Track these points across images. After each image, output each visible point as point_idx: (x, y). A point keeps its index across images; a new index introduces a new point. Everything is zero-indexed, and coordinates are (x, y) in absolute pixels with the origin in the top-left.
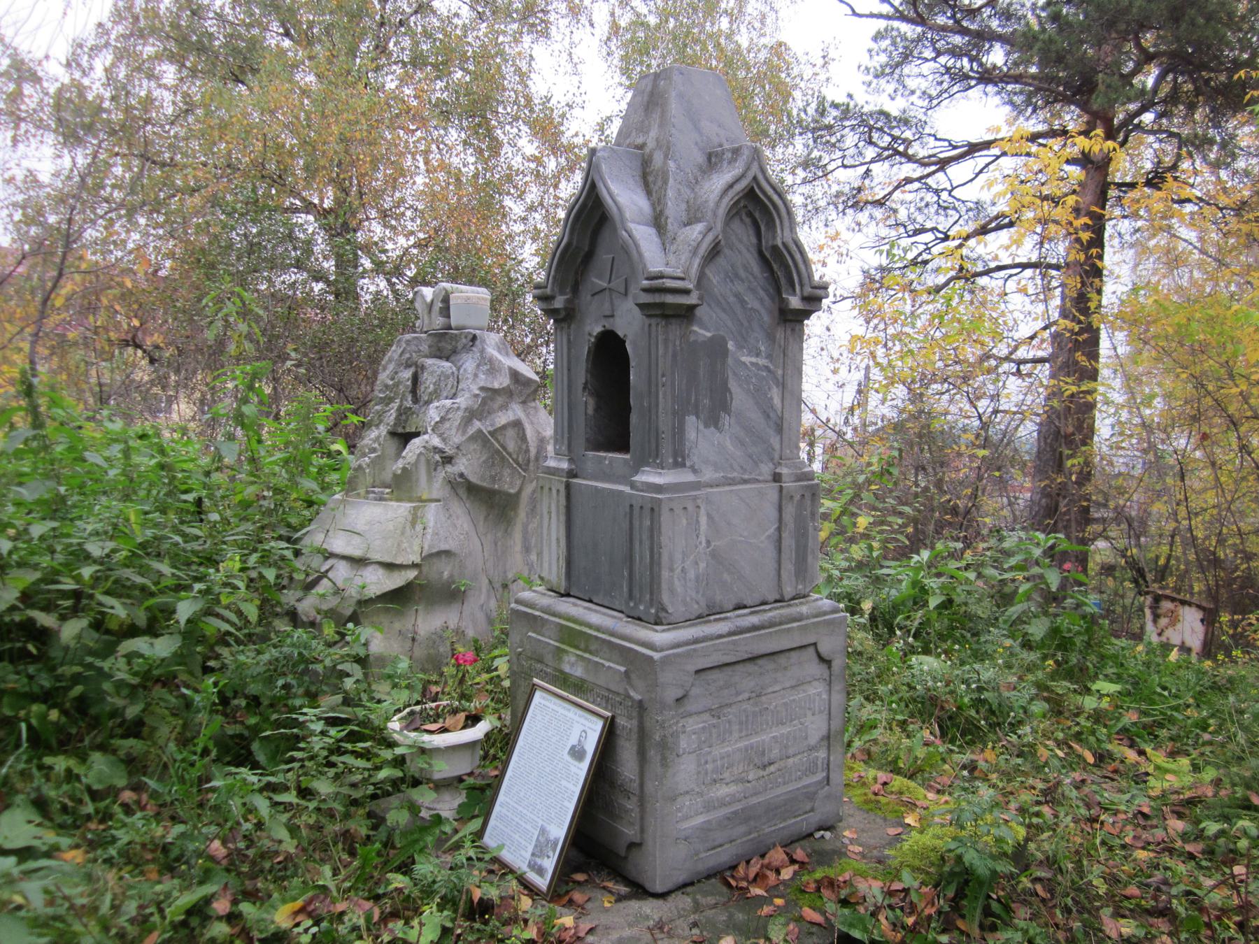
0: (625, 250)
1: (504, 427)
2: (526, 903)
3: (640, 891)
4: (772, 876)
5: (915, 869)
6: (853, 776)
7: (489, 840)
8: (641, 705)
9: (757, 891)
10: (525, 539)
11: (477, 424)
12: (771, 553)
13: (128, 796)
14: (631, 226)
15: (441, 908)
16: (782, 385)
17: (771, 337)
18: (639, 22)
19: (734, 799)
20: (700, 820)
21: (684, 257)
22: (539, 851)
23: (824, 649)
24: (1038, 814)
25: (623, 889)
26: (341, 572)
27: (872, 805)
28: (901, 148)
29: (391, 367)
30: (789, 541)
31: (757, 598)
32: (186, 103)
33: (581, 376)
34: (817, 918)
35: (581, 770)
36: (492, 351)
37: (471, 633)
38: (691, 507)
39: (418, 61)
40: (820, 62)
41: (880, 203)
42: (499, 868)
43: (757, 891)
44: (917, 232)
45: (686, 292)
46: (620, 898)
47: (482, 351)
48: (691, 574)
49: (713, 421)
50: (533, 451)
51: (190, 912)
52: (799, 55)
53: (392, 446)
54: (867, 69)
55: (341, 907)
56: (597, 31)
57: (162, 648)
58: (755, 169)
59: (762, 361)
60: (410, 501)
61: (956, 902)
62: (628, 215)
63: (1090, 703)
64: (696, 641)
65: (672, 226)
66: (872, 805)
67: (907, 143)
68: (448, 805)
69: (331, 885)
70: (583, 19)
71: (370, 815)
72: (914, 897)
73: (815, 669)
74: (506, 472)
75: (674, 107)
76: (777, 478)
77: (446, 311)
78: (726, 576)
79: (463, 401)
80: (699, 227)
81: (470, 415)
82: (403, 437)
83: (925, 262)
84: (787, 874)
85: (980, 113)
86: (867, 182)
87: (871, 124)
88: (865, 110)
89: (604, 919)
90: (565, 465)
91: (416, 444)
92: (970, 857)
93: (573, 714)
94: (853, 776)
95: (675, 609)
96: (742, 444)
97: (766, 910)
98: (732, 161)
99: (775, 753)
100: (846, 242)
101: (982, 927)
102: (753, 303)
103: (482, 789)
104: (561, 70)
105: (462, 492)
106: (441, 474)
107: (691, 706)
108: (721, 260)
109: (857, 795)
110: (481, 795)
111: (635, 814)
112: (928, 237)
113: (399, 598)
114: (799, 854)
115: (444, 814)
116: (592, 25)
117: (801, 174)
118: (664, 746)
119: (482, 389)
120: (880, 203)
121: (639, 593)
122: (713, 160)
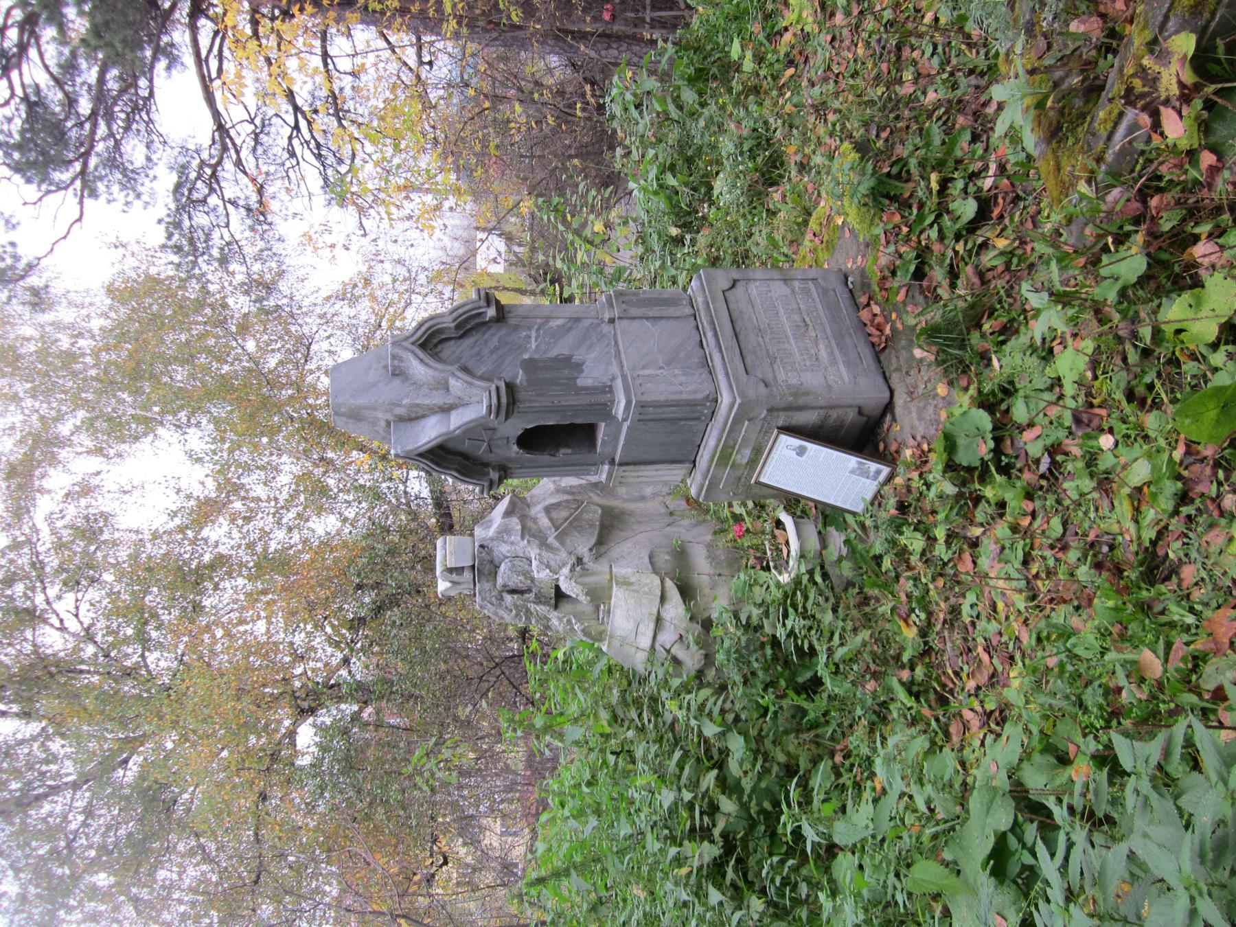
0: (465, 432)
1: (551, 520)
2: (898, 480)
3: (889, 407)
4: (878, 319)
5: (871, 224)
6: (809, 257)
7: (859, 508)
8: (771, 410)
9: (888, 331)
10: (635, 500)
11: (551, 540)
12: (663, 324)
13: (838, 758)
14: (452, 427)
15: (901, 533)
16: (548, 319)
17: (516, 328)
18: (89, 425)
19: (829, 346)
20: (843, 369)
21: (475, 391)
22: (865, 474)
23: (726, 285)
24: (834, 125)
25: (888, 418)
26: (667, 637)
27: (830, 246)
28: (208, 171)
29: (501, 612)
30: (655, 312)
31: (695, 332)
32: (195, 854)
33: (545, 458)
34: (903, 291)
35: (813, 448)
36: (492, 532)
37: (709, 537)
38: (638, 382)
39: (143, 640)
40: (121, 251)
41: (260, 191)
42: (877, 500)
43: (888, 331)
44: (293, 154)
45: (498, 388)
46: (894, 419)
47: (492, 539)
48: (683, 379)
49: (578, 367)
50: (567, 497)
51: (910, 693)
52: (115, 271)
53: (566, 607)
54: (127, 203)
55: (903, 598)
56: (104, 467)
57: (737, 744)
58: (407, 344)
59: (534, 334)
60: (611, 588)
61: (893, 199)
62: (444, 430)
63: (748, 65)
64: (727, 374)
65: (450, 400)
66: (830, 246)
67: (203, 163)
68: (837, 540)
69: (890, 605)
70: (95, 481)
71: (846, 589)
72: (890, 226)
73: (739, 291)
74: (585, 516)
75: (362, 401)
76: (612, 321)
77: (459, 570)
78: (682, 355)
79: (533, 552)
80: (452, 381)
81: (544, 544)
82: (560, 596)
83: (318, 146)
84: (876, 309)
85: (176, 98)
86: (241, 203)
87: (186, 199)
88: (173, 206)
89: (907, 430)
90: (606, 467)
91: (565, 586)
92: (863, 189)
93: (775, 455)
94: (809, 257)
95: (706, 389)
96: (591, 346)
97: (899, 326)
98: (401, 360)
99: (796, 317)
100: (312, 226)
101: (908, 181)
102: (494, 342)
103: (825, 517)
104: (140, 501)
105: (603, 549)
106: (591, 565)
107: (769, 377)
108: (470, 365)
109: (823, 256)
110: (829, 516)
111: (840, 411)
112: (296, 142)
113: (686, 592)
114: (863, 300)
115: (843, 538)
116: (99, 473)
117: (233, 267)
118: (796, 395)
119: (523, 538)
120: (260, 191)
121: (697, 413)
122: (398, 373)
